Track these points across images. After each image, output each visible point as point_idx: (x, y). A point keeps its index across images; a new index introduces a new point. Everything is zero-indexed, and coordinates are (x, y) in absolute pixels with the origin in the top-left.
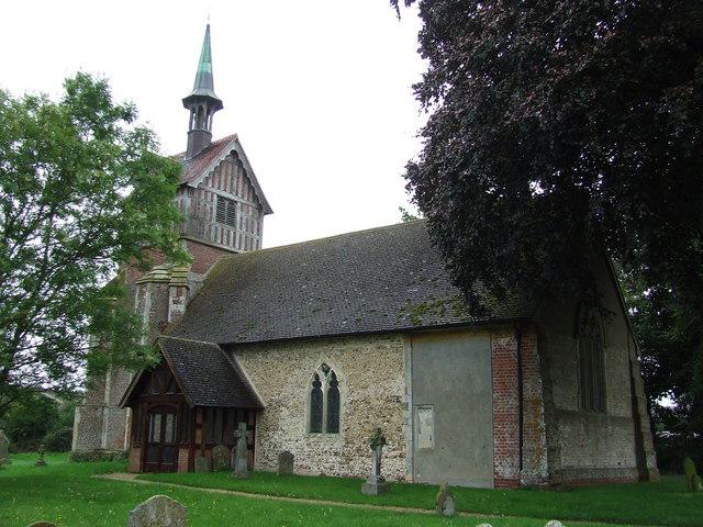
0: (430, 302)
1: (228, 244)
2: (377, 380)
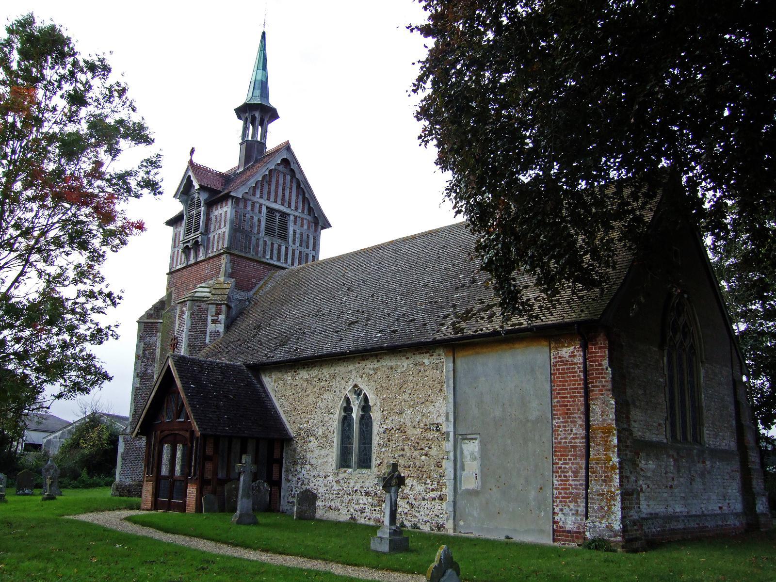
0: (479, 306)
1: (279, 259)
2: (412, 400)
